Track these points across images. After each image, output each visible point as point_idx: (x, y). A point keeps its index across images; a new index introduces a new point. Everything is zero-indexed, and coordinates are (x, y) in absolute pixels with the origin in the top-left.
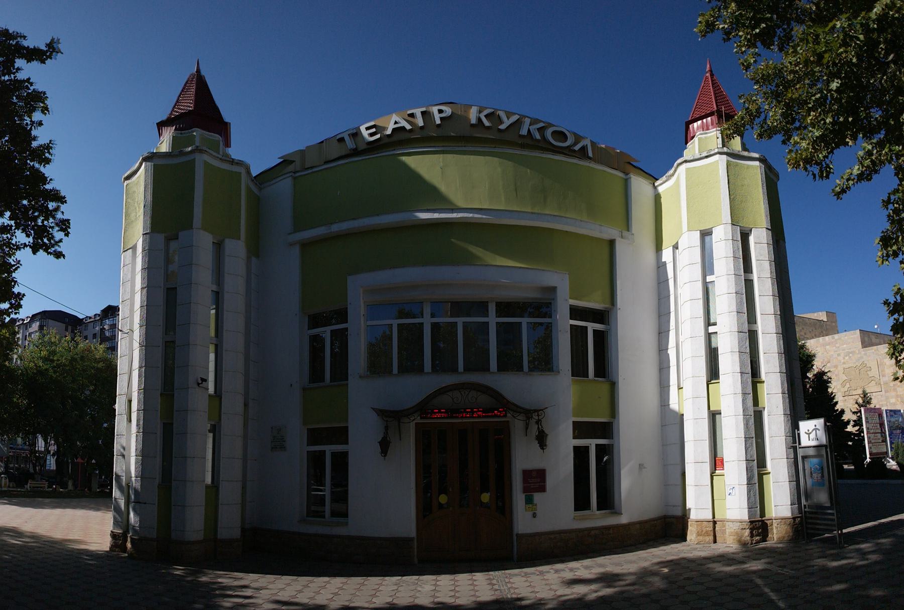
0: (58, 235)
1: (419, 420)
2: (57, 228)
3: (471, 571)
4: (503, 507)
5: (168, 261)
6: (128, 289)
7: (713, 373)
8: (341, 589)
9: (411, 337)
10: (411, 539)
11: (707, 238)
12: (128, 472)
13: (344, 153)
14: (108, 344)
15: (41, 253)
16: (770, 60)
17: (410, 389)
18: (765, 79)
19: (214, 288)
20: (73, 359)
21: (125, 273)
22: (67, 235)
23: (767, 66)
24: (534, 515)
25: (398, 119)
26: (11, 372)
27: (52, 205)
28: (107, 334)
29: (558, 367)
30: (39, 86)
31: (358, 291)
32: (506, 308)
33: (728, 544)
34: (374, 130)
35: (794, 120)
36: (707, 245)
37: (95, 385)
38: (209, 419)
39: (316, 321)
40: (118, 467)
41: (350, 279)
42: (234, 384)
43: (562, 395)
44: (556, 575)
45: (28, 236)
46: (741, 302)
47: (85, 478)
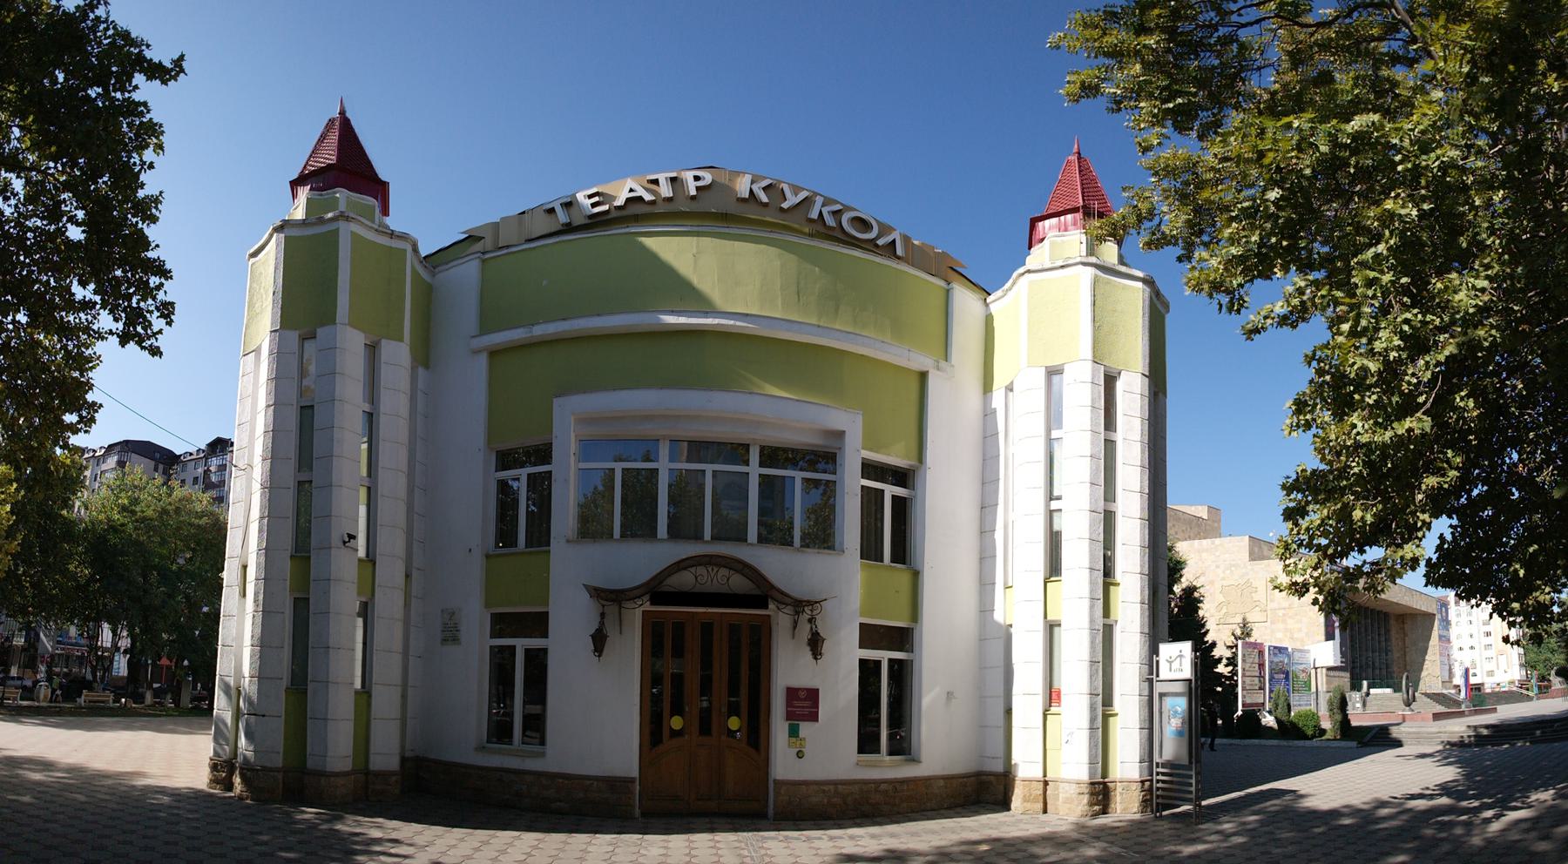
0: (158, 323)
1: (648, 607)
2: (156, 314)
3: (712, 830)
4: (757, 735)
5: (303, 373)
6: (248, 409)
7: (1054, 567)
8: (535, 847)
9: (640, 489)
10: (632, 780)
11: (1056, 379)
12: (239, 674)
13: (553, 229)
14: (214, 493)
15: (132, 346)
16: (1181, 148)
18: (1169, 172)
19: (367, 407)
20: (164, 511)
21: (244, 385)
22: (169, 323)
23: (1175, 155)
24: (800, 755)
25: (634, 186)
26: (69, 524)
27: (154, 281)
28: (214, 479)
29: (842, 543)
30: (155, 115)
31: (568, 422)
32: (772, 455)
33: (1069, 811)
34: (596, 199)
35: (1201, 232)
36: (1055, 388)
37: (194, 550)
38: (359, 594)
39: (506, 460)
40: (223, 667)
41: (558, 403)
42: (392, 544)
43: (845, 585)
44: (831, 844)
45: (116, 320)
46: (1097, 469)
47: (173, 680)
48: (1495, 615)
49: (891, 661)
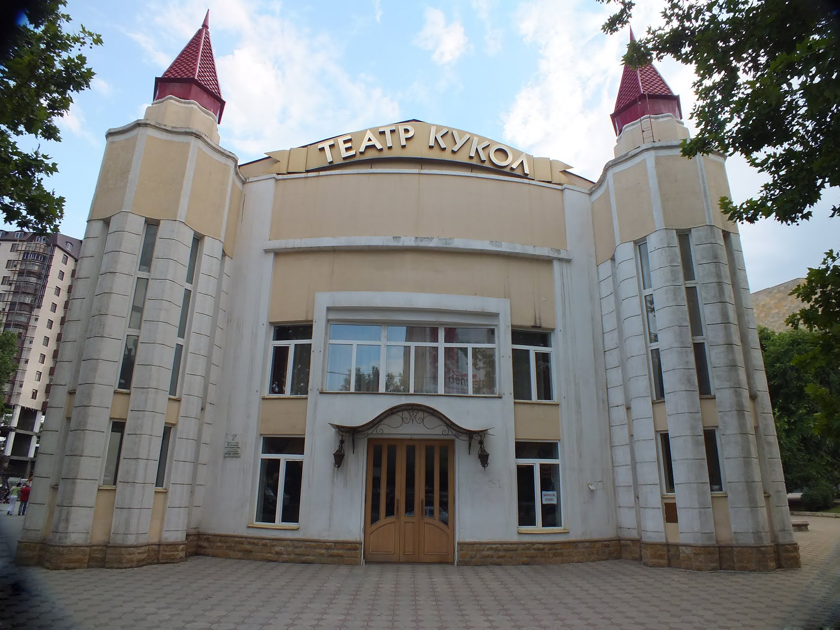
17: (363, 410)
48: (636, 537)
49: (541, 465)
